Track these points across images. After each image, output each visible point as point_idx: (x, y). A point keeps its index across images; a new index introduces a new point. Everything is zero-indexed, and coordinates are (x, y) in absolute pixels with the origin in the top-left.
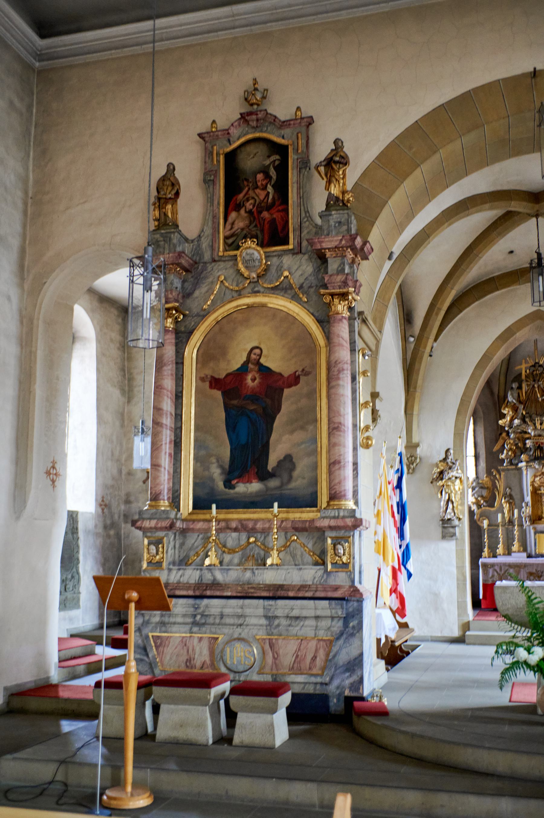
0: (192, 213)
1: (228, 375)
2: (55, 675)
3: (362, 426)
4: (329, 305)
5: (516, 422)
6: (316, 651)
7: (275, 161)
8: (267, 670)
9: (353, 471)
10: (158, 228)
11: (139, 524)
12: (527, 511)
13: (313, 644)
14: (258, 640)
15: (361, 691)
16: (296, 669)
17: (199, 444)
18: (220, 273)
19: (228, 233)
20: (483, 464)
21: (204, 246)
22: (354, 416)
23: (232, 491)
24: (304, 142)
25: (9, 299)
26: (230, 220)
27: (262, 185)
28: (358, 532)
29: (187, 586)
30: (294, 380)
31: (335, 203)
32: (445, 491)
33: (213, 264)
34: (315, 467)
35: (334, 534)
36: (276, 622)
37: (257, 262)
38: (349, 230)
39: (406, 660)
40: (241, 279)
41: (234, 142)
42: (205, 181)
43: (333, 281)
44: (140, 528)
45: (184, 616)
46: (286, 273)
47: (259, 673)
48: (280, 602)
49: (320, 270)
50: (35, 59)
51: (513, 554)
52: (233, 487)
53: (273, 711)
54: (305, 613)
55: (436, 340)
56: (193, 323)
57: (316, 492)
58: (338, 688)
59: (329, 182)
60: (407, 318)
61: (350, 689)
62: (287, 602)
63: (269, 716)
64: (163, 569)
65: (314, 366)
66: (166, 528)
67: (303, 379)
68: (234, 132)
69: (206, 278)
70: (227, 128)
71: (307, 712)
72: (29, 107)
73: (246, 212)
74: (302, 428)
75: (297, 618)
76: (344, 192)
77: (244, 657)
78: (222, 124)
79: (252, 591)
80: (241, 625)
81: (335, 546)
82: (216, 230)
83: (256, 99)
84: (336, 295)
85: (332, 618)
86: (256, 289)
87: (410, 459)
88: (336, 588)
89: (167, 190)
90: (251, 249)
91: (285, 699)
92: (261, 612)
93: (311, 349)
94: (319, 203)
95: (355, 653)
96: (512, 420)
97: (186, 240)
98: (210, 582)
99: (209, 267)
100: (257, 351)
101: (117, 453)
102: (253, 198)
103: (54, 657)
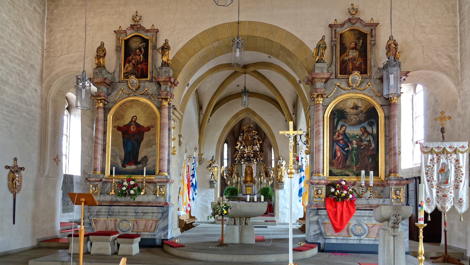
0: (112, 61)
1: (124, 126)
2: (59, 235)
3: (172, 146)
4: (161, 102)
5: (242, 147)
8: (135, 230)
10: (97, 67)
11: (88, 179)
12: (243, 179)
13: (151, 222)
16: (144, 230)
17: (113, 151)
20: (230, 162)
22: (169, 143)
25: (36, 90)
26: (126, 67)
29: (107, 202)
30: (148, 129)
34: (155, 161)
35: (160, 184)
36: (139, 214)
38: (169, 75)
39: (193, 229)
40: (130, 90)
42: (116, 50)
44: (89, 181)
45: (105, 212)
46: (146, 89)
47: (132, 232)
48: (140, 207)
52: (125, 167)
53: (132, 243)
54: (148, 211)
55: (211, 116)
57: (155, 170)
59: (163, 56)
65: (156, 124)
67: (151, 129)
68: (129, 32)
69: (116, 88)
71: (146, 245)
72: (44, 11)
74: (151, 146)
76: (168, 60)
77: (126, 227)
78: (124, 28)
82: (120, 70)
88: (160, 203)
89: (101, 52)
90: (133, 79)
91: (138, 239)
92: (133, 211)
93: (155, 118)
95: (165, 225)
96: (240, 147)
97: (109, 73)
99: (118, 84)
100: (135, 118)
101: (90, 153)
103: (58, 228)
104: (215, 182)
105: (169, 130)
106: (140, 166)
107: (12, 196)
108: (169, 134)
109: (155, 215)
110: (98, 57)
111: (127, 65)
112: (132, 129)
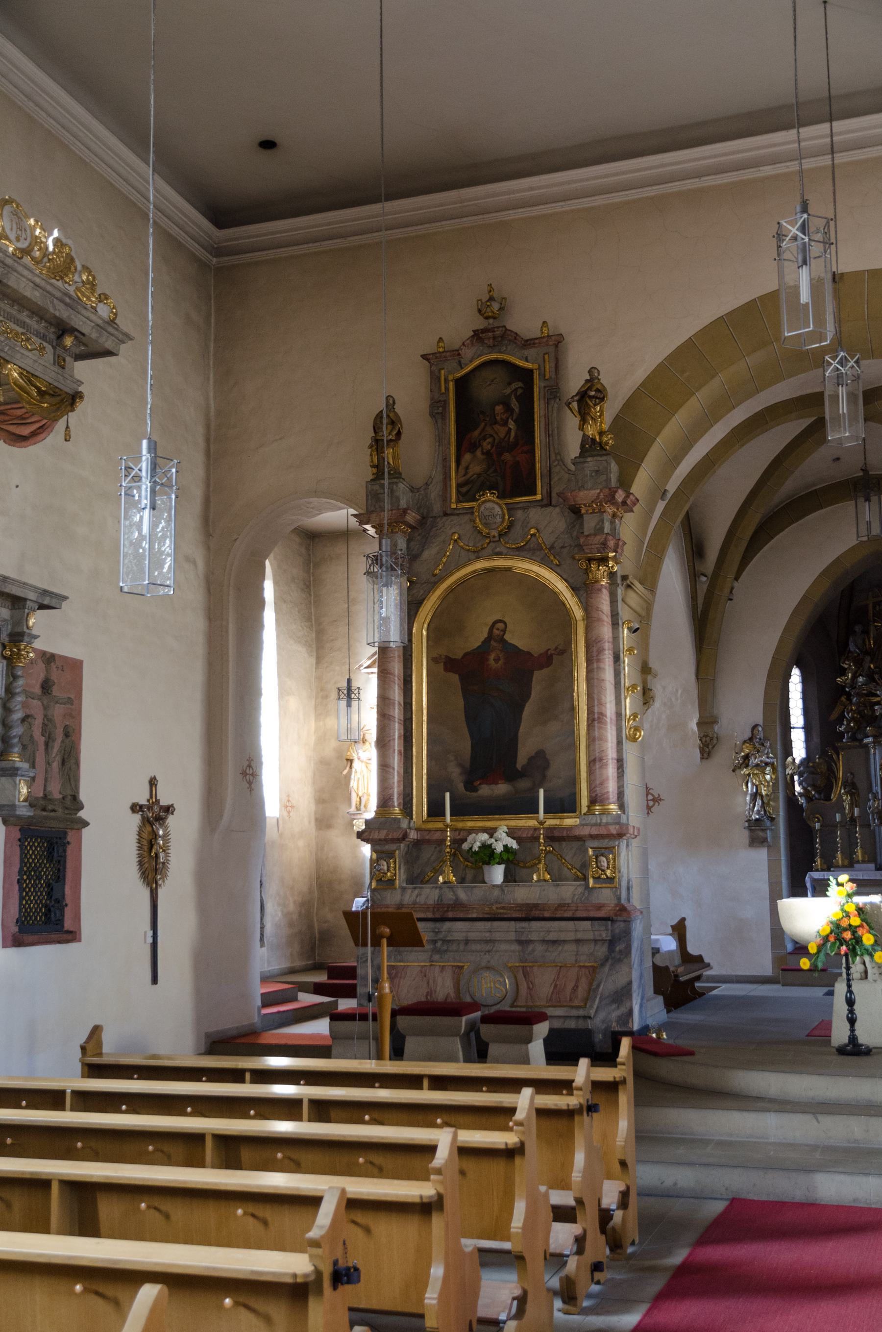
0: (422, 451)
1: (466, 655)
4: (587, 571)
6: (578, 980)
7: (516, 389)
9: (618, 769)
14: (510, 968)
15: (630, 1025)
18: (453, 530)
19: (461, 480)
20: (816, 739)
21: (433, 496)
23: (474, 794)
24: (553, 365)
26: (464, 463)
27: (502, 419)
28: (625, 841)
30: (546, 660)
31: (590, 447)
32: (752, 782)
33: (445, 518)
34: (574, 764)
35: (596, 844)
36: (530, 947)
37: (498, 517)
38: (608, 480)
41: (466, 365)
42: (432, 415)
43: (590, 542)
46: (532, 531)
48: (535, 925)
49: (575, 526)
50: (211, 254)
51: (855, 865)
52: (475, 790)
53: (529, 1040)
54: (563, 937)
56: (422, 592)
57: (575, 794)
58: (603, 1021)
59: (584, 421)
60: (695, 550)
61: (617, 1022)
62: (543, 923)
63: (524, 1046)
64: (395, 888)
66: (398, 839)
68: (467, 353)
70: (456, 347)
73: (483, 453)
75: (554, 942)
77: (493, 987)
79: (502, 911)
80: (489, 951)
81: (597, 858)
83: (493, 312)
84: (595, 560)
85: (596, 941)
86: (498, 550)
87: (704, 740)
88: (600, 907)
89: (386, 429)
90: (491, 504)
91: (542, 1029)
92: (512, 936)
94: (573, 449)
95: (622, 981)
96: (855, 677)
98: (451, 902)
100: (500, 626)
102: (491, 436)
104: (768, 823)
105: (617, 659)
106: (524, 784)
107: (146, 893)
108: (617, 673)
109: (586, 949)
110: (377, 445)
111: (467, 457)
112: (492, 662)
